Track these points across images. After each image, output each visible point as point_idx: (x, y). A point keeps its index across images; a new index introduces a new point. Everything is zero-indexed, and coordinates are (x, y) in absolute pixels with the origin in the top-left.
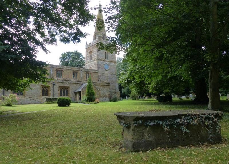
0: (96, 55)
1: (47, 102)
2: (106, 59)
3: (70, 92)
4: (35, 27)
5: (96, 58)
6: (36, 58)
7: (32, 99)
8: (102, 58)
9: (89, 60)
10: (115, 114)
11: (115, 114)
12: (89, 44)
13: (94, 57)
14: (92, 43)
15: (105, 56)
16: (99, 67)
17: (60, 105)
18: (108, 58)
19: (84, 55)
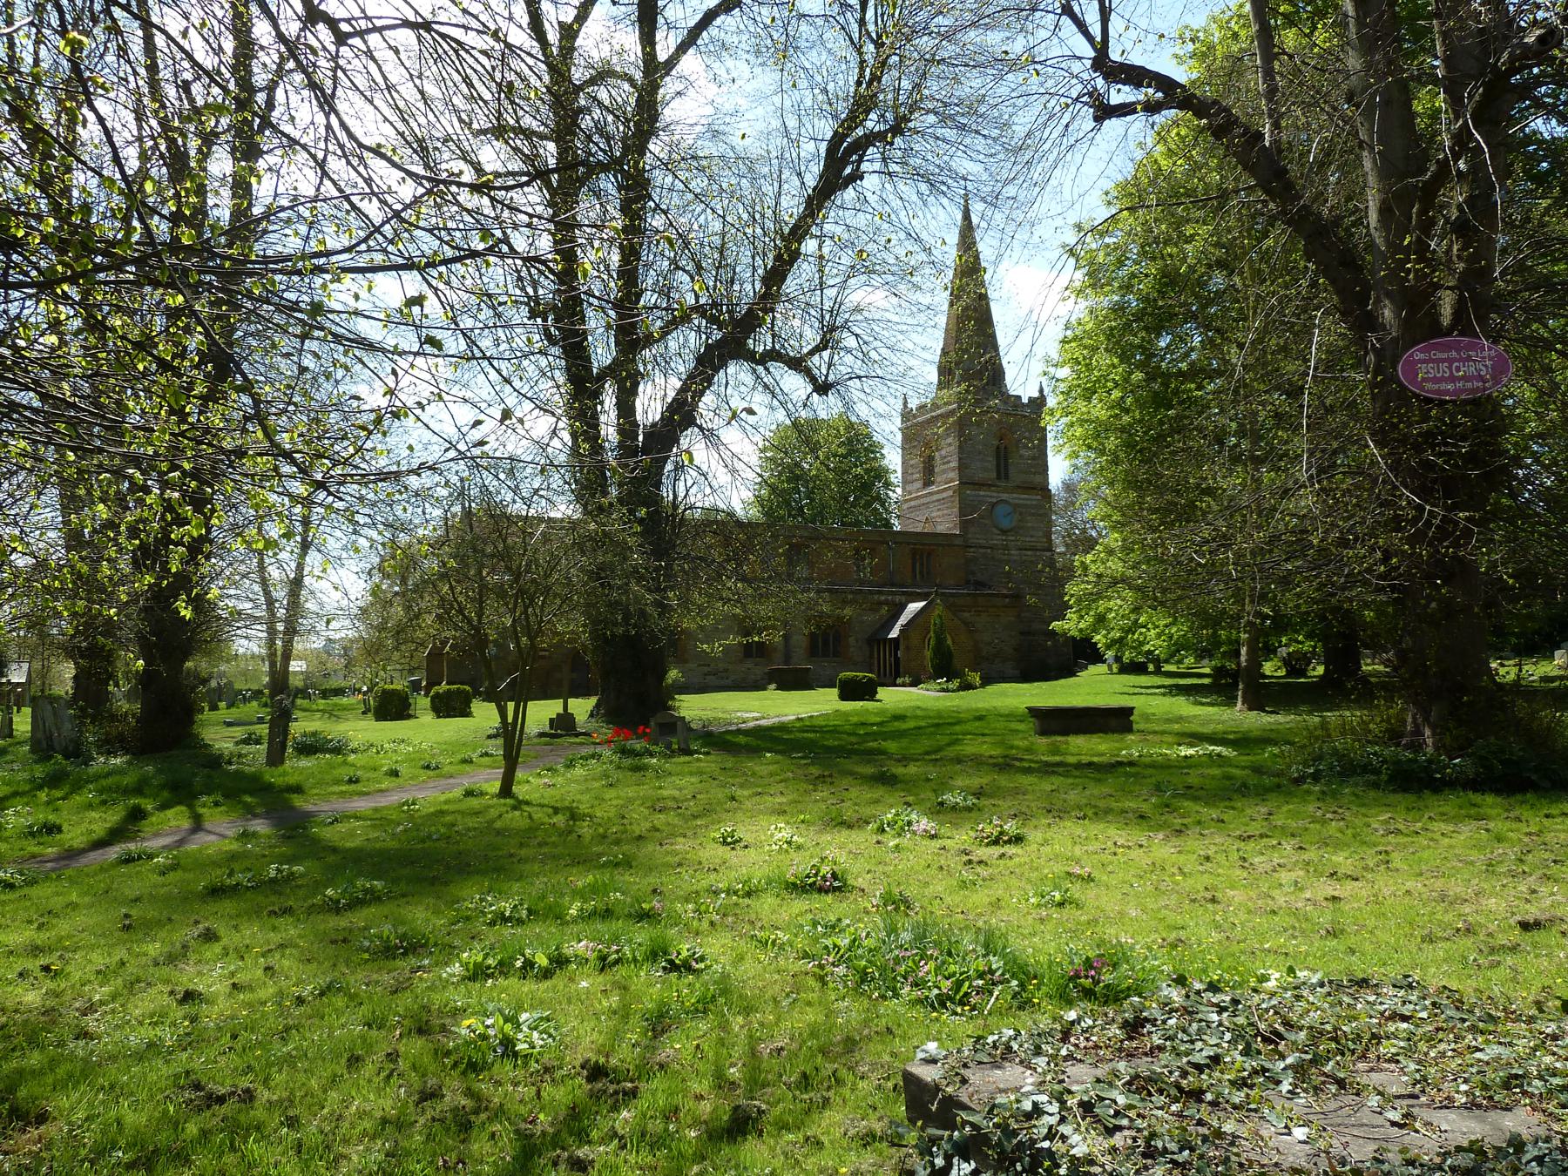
0: (954, 464)
1: (49, 767)
2: (999, 477)
3: (852, 640)
4: (754, 147)
5: (954, 475)
6: (1176, 56)
7: (709, 674)
8: (980, 476)
9: (919, 484)
10: (489, 737)
11: (489, 737)
12: (922, 407)
13: (944, 471)
14: (935, 406)
15: (998, 465)
16: (964, 525)
17: (844, 697)
18: (1012, 471)
19: (893, 459)
